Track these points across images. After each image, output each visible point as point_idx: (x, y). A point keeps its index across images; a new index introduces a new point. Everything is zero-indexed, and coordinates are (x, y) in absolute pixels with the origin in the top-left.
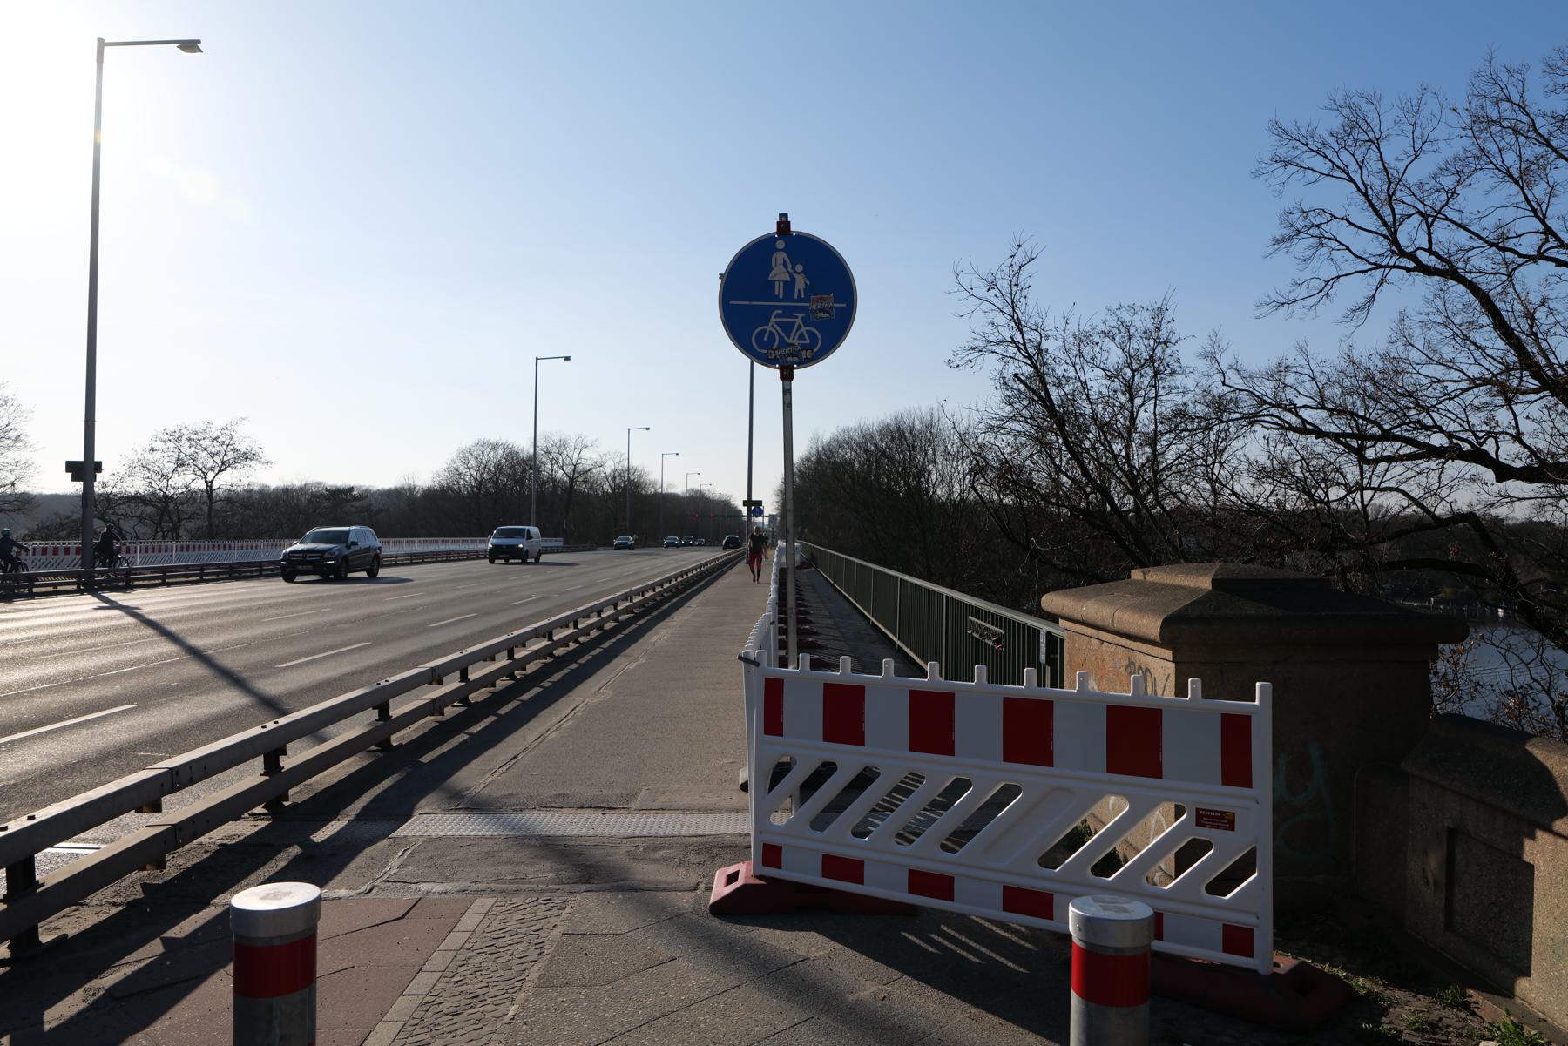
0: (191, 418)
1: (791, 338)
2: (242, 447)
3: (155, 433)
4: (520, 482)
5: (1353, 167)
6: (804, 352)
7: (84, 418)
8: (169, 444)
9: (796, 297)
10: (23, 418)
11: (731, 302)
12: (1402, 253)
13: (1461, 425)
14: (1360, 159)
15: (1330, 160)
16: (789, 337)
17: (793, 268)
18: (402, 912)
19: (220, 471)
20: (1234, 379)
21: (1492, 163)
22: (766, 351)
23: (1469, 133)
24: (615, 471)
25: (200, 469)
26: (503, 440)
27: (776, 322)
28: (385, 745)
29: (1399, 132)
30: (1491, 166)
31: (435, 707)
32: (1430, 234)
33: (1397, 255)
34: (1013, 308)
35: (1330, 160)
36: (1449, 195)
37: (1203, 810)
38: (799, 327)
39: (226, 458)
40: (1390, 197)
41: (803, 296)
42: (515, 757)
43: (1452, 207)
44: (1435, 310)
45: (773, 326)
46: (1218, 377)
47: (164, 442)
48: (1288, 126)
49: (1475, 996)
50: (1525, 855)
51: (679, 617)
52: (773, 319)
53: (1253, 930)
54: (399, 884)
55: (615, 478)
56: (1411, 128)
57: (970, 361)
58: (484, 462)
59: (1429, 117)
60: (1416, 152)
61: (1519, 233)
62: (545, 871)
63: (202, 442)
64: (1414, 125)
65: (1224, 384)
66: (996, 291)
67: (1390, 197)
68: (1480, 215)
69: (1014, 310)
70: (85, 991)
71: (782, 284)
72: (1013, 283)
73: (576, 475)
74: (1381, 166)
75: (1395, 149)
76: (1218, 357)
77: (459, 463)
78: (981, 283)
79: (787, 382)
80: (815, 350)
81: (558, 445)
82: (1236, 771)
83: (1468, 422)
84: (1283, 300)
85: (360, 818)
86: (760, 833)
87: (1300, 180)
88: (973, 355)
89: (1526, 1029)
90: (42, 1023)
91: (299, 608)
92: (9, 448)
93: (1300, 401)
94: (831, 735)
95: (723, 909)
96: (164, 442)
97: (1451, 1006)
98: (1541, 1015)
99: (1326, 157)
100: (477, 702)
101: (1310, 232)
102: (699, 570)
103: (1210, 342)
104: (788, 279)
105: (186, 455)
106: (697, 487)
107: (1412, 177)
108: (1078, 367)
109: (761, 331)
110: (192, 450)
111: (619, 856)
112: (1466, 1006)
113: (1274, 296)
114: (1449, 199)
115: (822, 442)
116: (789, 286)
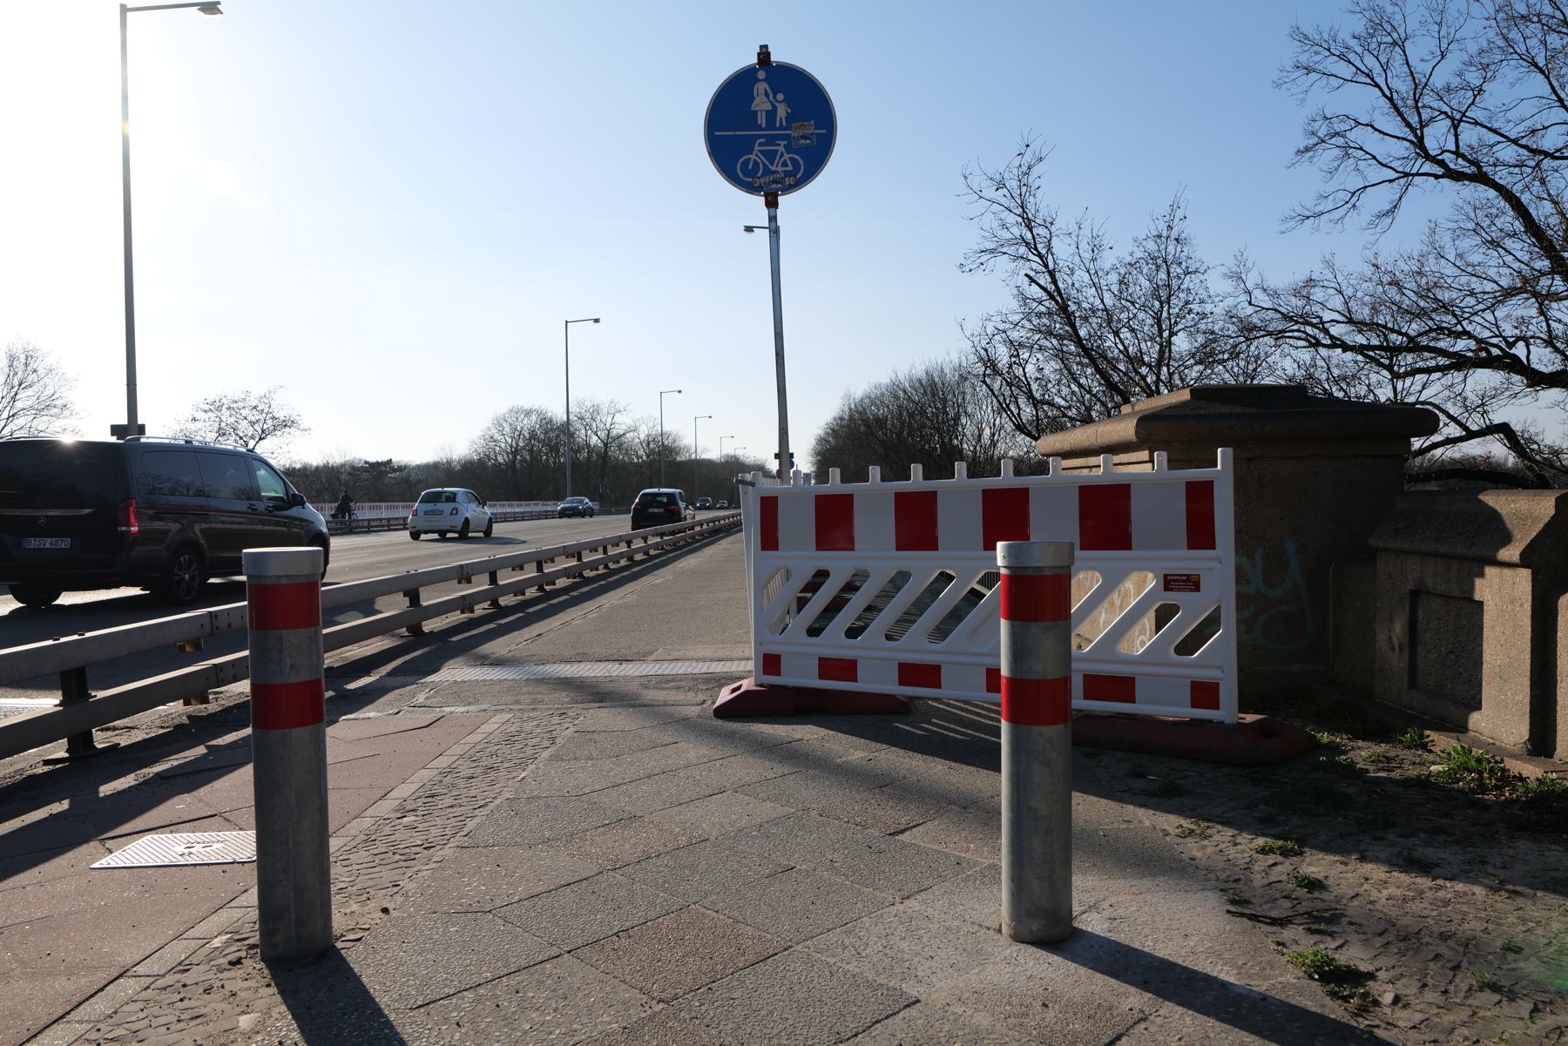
0: (231, 389)
1: (775, 166)
2: (281, 415)
3: (196, 403)
4: (554, 449)
5: (1377, 70)
6: (787, 179)
7: (125, 382)
8: (210, 413)
9: (778, 125)
10: (67, 387)
11: (716, 133)
12: (1428, 157)
13: (1491, 331)
14: (1383, 60)
15: (1354, 65)
16: (772, 165)
17: (775, 97)
18: (427, 724)
19: (261, 439)
20: (1261, 299)
21: (1516, 52)
22: (751, 180)
23: (1493, 23)
24: (648, 436)
25: (241, 438)
26: (536, 407)
27: (759, 151)
28: (416, 630)
29: (1425, 32)
30: (1516, 56)
31: (465, 604)
32: (1456, 136)
33: (1423, 158)
34: (1022, 207)
35: (1354, 65)
36: (1476, 93)
37: (1170, 575)
38: (782, 155)
39: (265, 427)
40: (1417, 102)
41: (784, 124)
42: (539, 635)
43: (1479, 105)
44: (1464, 217)
45: (757, 155)
46: (1244, 297)
47: (205, 411)
48: (1310, 32)
49: (1432, 735)
50: (1476, 595)
51: (709, 551)
52: (756, 148)
53: (1218, 684)
54: (424, 708)
55: (649, 443)
56: (1437, 27)
57: (982, 264)
58: (519, 428)
59: (1456, 15)
60: (1443, 53)
61: (1546, 125)
62: (563, 696)
63: (242, 411)
64: (1440, 24)
65: (1250, 304)
66: (1004, 191)
67: (1417, 102)
68: (1505, 108)
69: (1024, 211)
70: (136, 775)
71: (764, 113)
72: (1022, 183)
73: (610, 440)
74: (1407, 69)
75: (1420, 50)
76: (1244, 277)
77: (494, 431)
78: (989, 183)
79: (772, 210)
80: (798, 177)
81: (591, 411)
82: (1200, 534)
83: (1498, 327)
84: (1308, 214)
85: (389, 674)
86: (761, 644)
87: (1323, 88)
88: (985, 258)
89: (1474, 750)
90: (98, 793)
91: (339, 554)
92: (56, 416)
93: (1327, 316)
94: (823, 543)
95: (724, 712)
96: (205, 411)
97: (1409, 748)
98: (1491, 741)
99: (1350, 62)
100: (507, 606)
101: (1333, 141)
102: (731, 519)
103: (1235, 262)
104: (770, 108)
105: (227, 425)
106: (732, 452)
107: (1438, 81)
108: (1092, 272)
109: (745, 160)
110: (232, 420)
111: (633, 687)
112: (1424, 747)
113: (1299, 210)
114: (1475, 96)
115: (854, 399)
116: (771, 115)
